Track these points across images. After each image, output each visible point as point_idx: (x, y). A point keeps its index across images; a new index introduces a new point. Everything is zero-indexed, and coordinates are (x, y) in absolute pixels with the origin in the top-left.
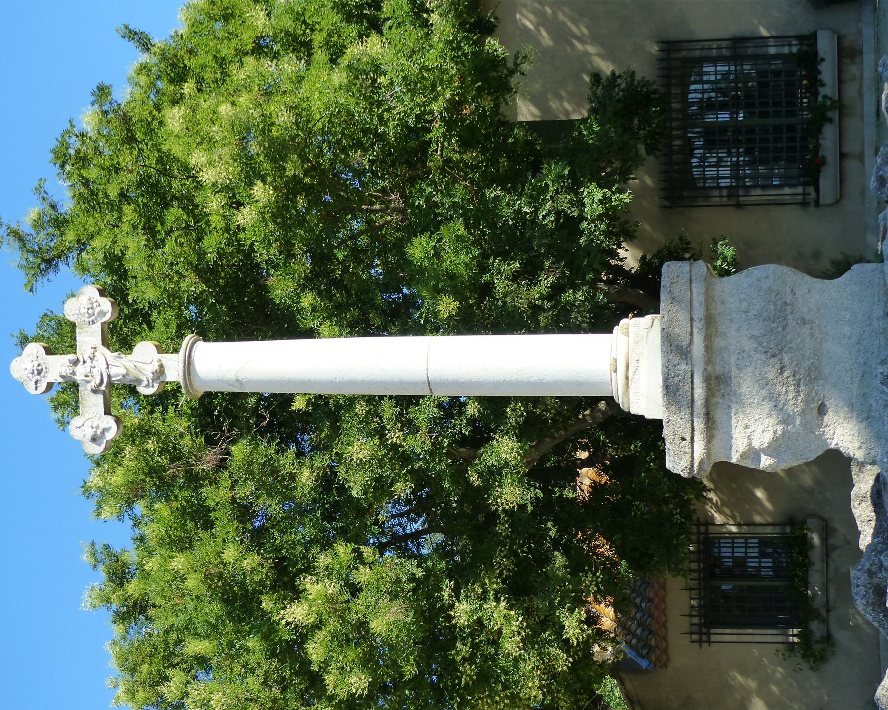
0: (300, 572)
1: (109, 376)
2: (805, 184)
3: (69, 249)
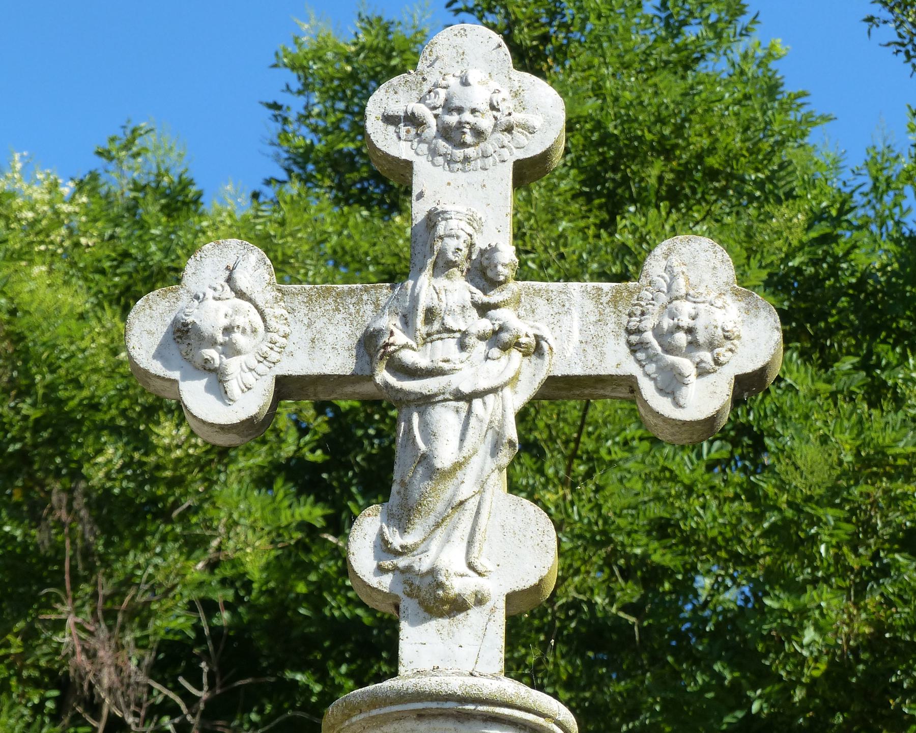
1: (425, 401)
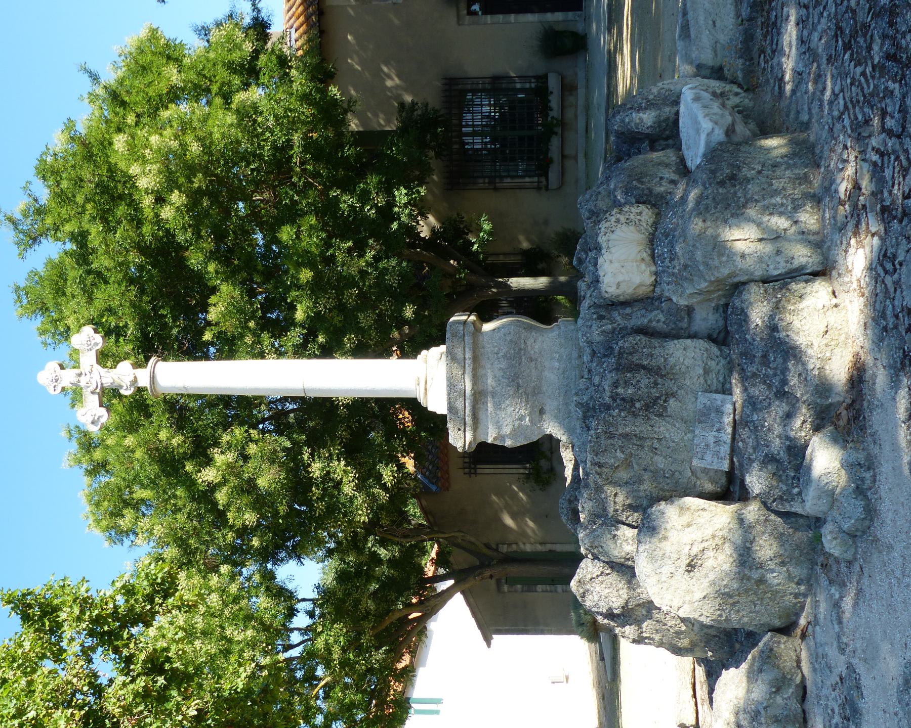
0: (210, 446)
1: (102, 384)
2: (540, 176)
3: (48, 229)
